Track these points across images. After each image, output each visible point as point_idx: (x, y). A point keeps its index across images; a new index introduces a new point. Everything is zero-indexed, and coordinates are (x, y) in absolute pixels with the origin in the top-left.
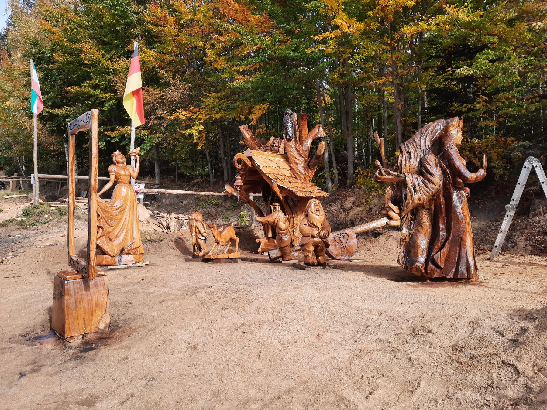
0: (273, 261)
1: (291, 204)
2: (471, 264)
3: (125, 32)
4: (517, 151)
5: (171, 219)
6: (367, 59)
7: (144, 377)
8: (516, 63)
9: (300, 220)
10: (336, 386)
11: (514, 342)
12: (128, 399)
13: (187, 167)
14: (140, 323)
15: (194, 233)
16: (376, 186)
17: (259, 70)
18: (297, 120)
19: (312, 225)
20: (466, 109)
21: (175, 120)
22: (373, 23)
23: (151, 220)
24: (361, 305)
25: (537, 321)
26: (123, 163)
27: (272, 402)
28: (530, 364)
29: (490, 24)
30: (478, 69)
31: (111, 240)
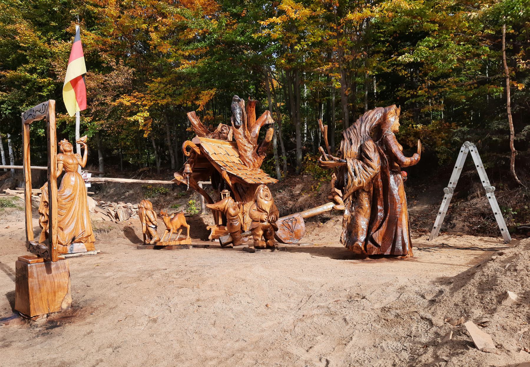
0: (224, 246)
1: (241, 191)
2: (407, 241)
3: (62, 12)
4: (456, 136)
5: (120, 208)
6: (314, 44)
7: (110, 346)
8: (455, 51)
9: (249, 206)
10: (282, 344)
11: (432, 302)
12: (98, 364)
13: (132, 156)
14: (101, 303)
15: (144, 222)
16: (324, 172)
17: (206, 55)
18: (245, 107)
19: (261, 210)
20: (410, 95)
21: (118, 106)
22: (319, 9)
23: (98, 209)
24: (305, 279)
25: (452, 284)
26: (70, 151)
27: (227, 359)
28: (442, 318)
29: (432, 11)
30: (418, 56)
31: (62, 229)
